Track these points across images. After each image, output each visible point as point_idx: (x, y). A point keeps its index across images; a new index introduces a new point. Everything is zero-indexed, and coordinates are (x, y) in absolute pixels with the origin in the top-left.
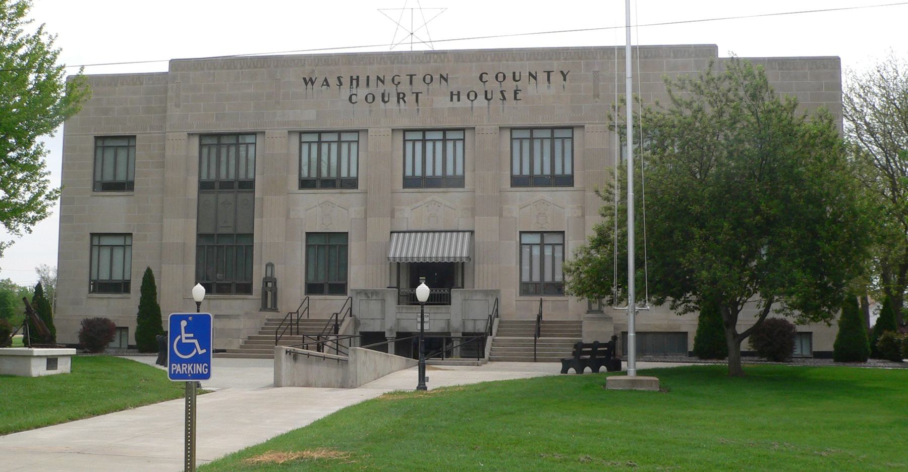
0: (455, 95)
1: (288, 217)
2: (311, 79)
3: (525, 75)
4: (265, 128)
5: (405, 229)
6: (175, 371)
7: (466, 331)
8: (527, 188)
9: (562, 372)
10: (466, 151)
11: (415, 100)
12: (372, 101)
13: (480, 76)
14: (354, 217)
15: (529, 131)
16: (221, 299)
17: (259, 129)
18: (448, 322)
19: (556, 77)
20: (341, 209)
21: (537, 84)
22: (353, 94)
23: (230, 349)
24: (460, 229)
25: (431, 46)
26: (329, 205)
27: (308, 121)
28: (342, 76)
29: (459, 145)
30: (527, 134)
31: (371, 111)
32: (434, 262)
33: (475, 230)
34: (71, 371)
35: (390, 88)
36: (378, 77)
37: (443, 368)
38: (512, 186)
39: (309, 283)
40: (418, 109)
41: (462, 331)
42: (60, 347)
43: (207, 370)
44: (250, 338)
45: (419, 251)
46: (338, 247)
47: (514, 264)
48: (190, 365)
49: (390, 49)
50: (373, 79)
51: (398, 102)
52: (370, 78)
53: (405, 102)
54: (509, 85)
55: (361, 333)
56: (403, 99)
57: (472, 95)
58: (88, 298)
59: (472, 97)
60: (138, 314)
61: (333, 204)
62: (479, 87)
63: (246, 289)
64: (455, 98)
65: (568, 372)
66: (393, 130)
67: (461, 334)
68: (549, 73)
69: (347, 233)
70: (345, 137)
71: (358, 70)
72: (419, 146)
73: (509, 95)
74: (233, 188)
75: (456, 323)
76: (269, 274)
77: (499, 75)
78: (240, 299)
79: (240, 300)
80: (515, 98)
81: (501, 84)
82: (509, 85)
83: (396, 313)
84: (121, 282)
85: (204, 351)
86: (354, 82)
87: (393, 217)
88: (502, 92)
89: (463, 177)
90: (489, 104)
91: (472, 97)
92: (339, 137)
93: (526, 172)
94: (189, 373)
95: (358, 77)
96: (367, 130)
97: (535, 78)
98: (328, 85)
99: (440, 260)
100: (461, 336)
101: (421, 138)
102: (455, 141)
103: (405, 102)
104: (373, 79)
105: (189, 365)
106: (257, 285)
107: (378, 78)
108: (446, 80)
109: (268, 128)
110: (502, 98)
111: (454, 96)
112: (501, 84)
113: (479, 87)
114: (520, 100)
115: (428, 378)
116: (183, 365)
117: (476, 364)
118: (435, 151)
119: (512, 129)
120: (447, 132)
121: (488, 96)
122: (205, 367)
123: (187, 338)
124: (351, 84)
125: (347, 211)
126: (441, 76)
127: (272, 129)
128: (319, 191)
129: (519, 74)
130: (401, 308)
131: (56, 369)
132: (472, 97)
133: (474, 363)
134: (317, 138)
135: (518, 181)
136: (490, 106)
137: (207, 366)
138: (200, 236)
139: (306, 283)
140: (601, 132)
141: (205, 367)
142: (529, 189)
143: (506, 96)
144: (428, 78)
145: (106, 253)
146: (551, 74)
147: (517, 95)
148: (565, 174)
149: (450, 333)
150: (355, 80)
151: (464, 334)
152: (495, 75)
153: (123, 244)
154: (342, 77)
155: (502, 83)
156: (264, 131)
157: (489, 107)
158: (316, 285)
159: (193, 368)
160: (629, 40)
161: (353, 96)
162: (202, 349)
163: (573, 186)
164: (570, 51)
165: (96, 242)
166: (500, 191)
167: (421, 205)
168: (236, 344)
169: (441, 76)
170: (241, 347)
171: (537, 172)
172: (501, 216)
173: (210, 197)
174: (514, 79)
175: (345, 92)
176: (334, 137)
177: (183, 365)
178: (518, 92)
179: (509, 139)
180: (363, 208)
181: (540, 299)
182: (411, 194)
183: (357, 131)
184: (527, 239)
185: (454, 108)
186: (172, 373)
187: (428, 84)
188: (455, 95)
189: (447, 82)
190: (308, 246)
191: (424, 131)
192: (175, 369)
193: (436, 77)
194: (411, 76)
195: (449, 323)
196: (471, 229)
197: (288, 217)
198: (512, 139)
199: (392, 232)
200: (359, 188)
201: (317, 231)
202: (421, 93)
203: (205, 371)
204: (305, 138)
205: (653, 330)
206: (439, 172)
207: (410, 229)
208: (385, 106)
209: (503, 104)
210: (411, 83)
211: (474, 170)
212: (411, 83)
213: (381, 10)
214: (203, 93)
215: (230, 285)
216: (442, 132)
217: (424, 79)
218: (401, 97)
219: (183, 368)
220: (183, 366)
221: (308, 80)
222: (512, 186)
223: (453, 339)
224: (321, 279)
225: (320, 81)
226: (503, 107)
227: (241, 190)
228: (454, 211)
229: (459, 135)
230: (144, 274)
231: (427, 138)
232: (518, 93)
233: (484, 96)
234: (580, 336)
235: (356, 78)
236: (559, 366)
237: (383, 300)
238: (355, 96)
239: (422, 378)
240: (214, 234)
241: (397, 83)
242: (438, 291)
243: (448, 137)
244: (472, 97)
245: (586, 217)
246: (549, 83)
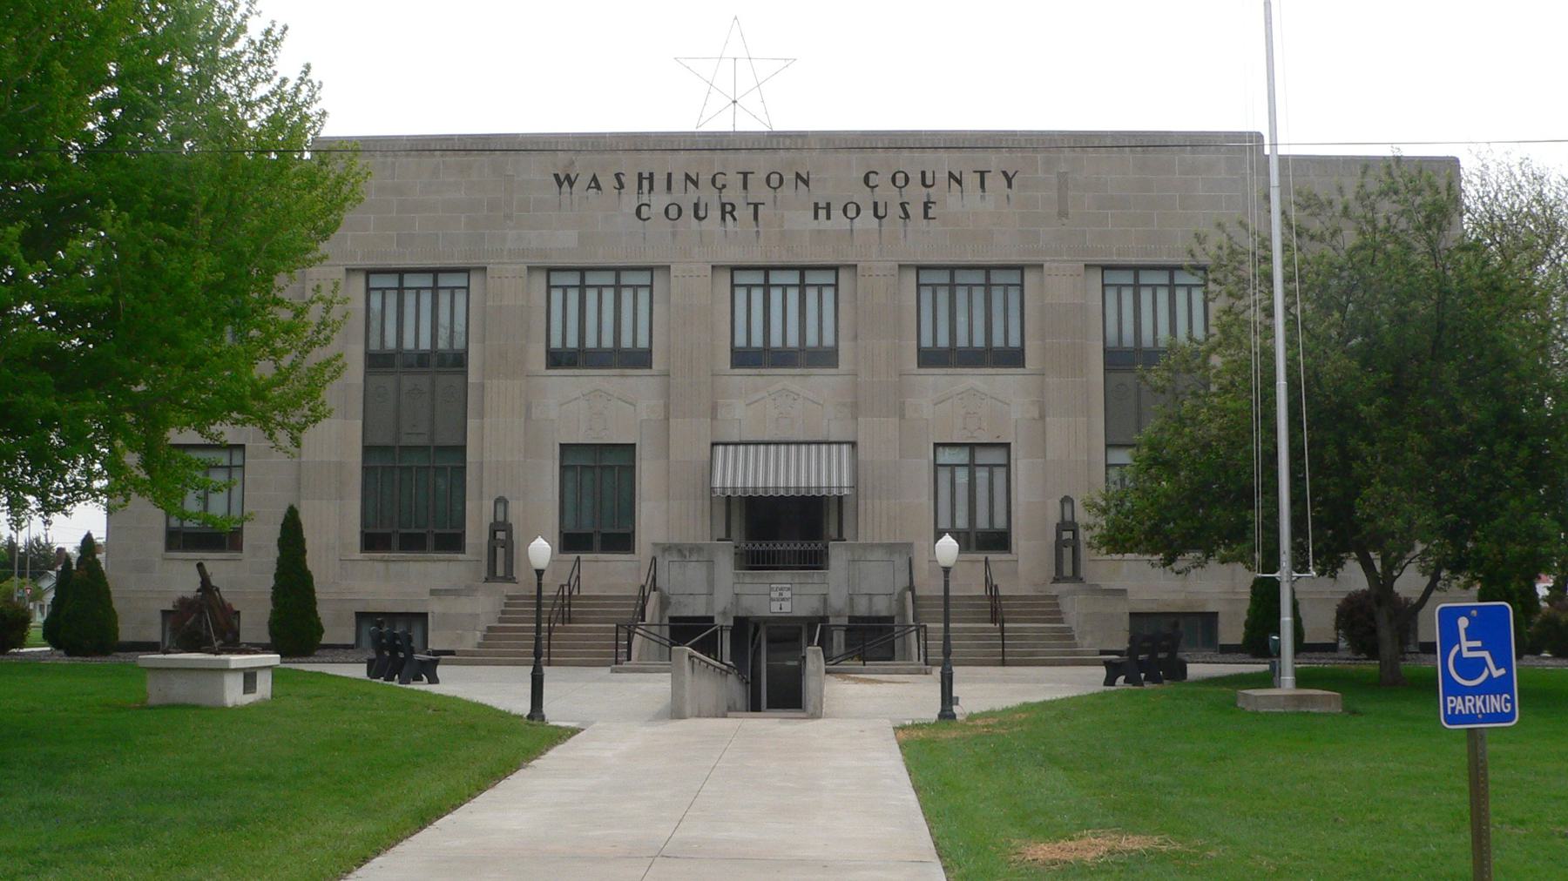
1: (528, 417)
2: (568, 177)
3: (942, 176)
5: (736, 439)
6: (1453, 709)
7: (857, 614)
8: (572, 371)
9: (1105, 684)
10: (840, 305)
11: (752, 217)
12: (676, 217)
13: (865, 177)
14: (646, 418)
15: (948, 272)
16: (409, 561)
17: (473, 262)
18: (825, 598)
19: (995, 182)
20: (628, 405)
21: (962, 192)
23: (461, 649)
24: (832, 439)
25: (768, 124)
26: (601, 396)
27: (564, 248)
28: (623, 172)
29: (828, 294)
30: (944, 277)
31: (674, 234)
32: (771, 496)
33: (859, 441)
34: (272, 696)
35: (708, 195)
36: (950, 173)
37: (884, 679)
38: (919, 366)
39: (566, 532)
40: (758, 232)
41: (848, 614)
42: (248, 652)
43: (1509, 705)
44: (490, 629)
45: (808, 478)
46: (617, 468)
47: (926, 501)
48: (1479, 697)
49: (697, 128)
50: (678, 178)
51: (723, 218)
52: (674, 177)
53: (735, 219)
54: (916, 193)
55: (672, 619)
56: (731, 213)
57: (851, 209)
58: (166, 559)
59: (852, 212)
60: (273, 588)
61: (609, 395)
62: (863, 196)
63: (452, 542)
64: (822, 213)
65: (1117, 684)
66: (713, 267)
67: (847, 619)
68: (982, 174)
69: (634, 445)
70: (627, 278)
71: (648, 163)
72: (757, 295)
73: (916, 210)
74: (393, 366)
75: (838, 601)
76: (500, 518)
77: (897, 175)
78: (444, 561)
79: (442, 563)
80: (926, 216)
81: (901, 192)
82: (916, 193)
83: (734, 583)
85: (1502, 671)
86: (646, 183)
87: (714, 417)
88: (903, 205)
89: (650, 351)
90: (880, 226)
91: (852, 213)
92: (583, 279)
93: (943, 341)
94: (1478, 712)
95: (651, 175)
96: (669, 267)
97: (959, 182)
98: (598, 187)
99: (803, 492)
100: (847, 623)
101: (762, 281)
102: (820, 287)
103: (735, 219)
104: (678, 178)
105: (1477, 697)
106: (476, 533)
107: (688, 177)
108: (806, 182)
109: (492, 261)
110: (903, 216)
111: (820, 211)
112: (901, 192)
113: (863, 196)
114: (934, 218)
115: (957, 698)
116: (1467, 698)
117: (923, 671)
118: (784, 304)
119: (920, 268)
120: (406, 276)
121: (879, 210)
122: (1506, 700)
123: (1470, 649)
124: (640, 186)
125: (632, 408)
126: (798, 176)
127: (499, 263)
128: (583, 372)
129: (932, 175)
130: (742, 575)
131: (254, 692)
132: (852, 213)
133: (921, 669)
134: (763, 278)
135: (930, 358)
136: (883, 228)
137: (1508, 697)
138: (368, 450)
139: (561, 532)
140: (1071, 275)
141: (1507, 701)
142: (950, 371)
144: (775, 179)
146: (986, 175)
147: (930, 211)
148: (638, 346)
149: (828, 617)
150: (646, 180)
151: (852, 619)
152: (891, 176)
153: (228, 464)
154: (623, 174)
155: (903, 189)
156: (1040, 263)
157: (880, 231)
158: (579, 535)
159: (1484, 702)
160: (1273, 123)
161: (643, 208)
162: (1498, 668)
163: (1023, 366)
164: (1018, 137)
166: (900, 375)
167: (763, 398)
168: (472, 640)
169: (798, 176)
170: (480, 645)
171: (962, 342)
172: (902, 416)
173: (387, 382)
174: (924, 184)
175: (630, 200)
176: (609, 278)
177: (1467, 698)
178: (930, 205)
179: (915, 285)
180: (662, 402)
181: (984, 559)
182: (746, 378)
183: (651, 269)
184: (946, 456)
185: (819, 231)
186: (1449, 713)
187: (775, 188)
188: (821, 208)
189: (808, 186)
190: (563, 468)
191: (767, 269)
192: (1453, 705)
193: (789, 177)
194: (745, 175)
195: (825, 601)
196: (851, 439)
197: (528, 417)
198: (919, 286)
199: (714, 444)
200: (654, 366)
201: (580, 442)
202: (763, 204)
203: (1506, 707)
204: (557, 279)
205: (1161, 610)
206: (793, 341)
207: (745, 438)
208: (700, 225)
209: (905, 225)
210: (745, 187)
211: (856, 337)
212: (745, 187)
213: (681, 60)
214: (373, 198)
215: (423, 536)
216: (432, 275)
217: (894, 180)
218: (727, 210)
219: (1467, 704)
220: (1467, 701)
221: (562, 178)
222: (733, 366)
223: (833, 628)
224: (587, 527)
225: (583, 181)
226: (905, 231)
228: (820, 407)
229: (643, 278)
230: (283, 517)
231: (587, 283)
232: (930, 208)
233: (872, 212)
234: (1061, 621)
235: (648, 176)
236: (1102, 672)
237: (711, 562)
238: (647, 207)
239: (948, 698)
240: (394, 447)
241: (720, 186)
242: (813, 545)
243: (808, 281)
244: (852, 212)
245: (1048, 419)
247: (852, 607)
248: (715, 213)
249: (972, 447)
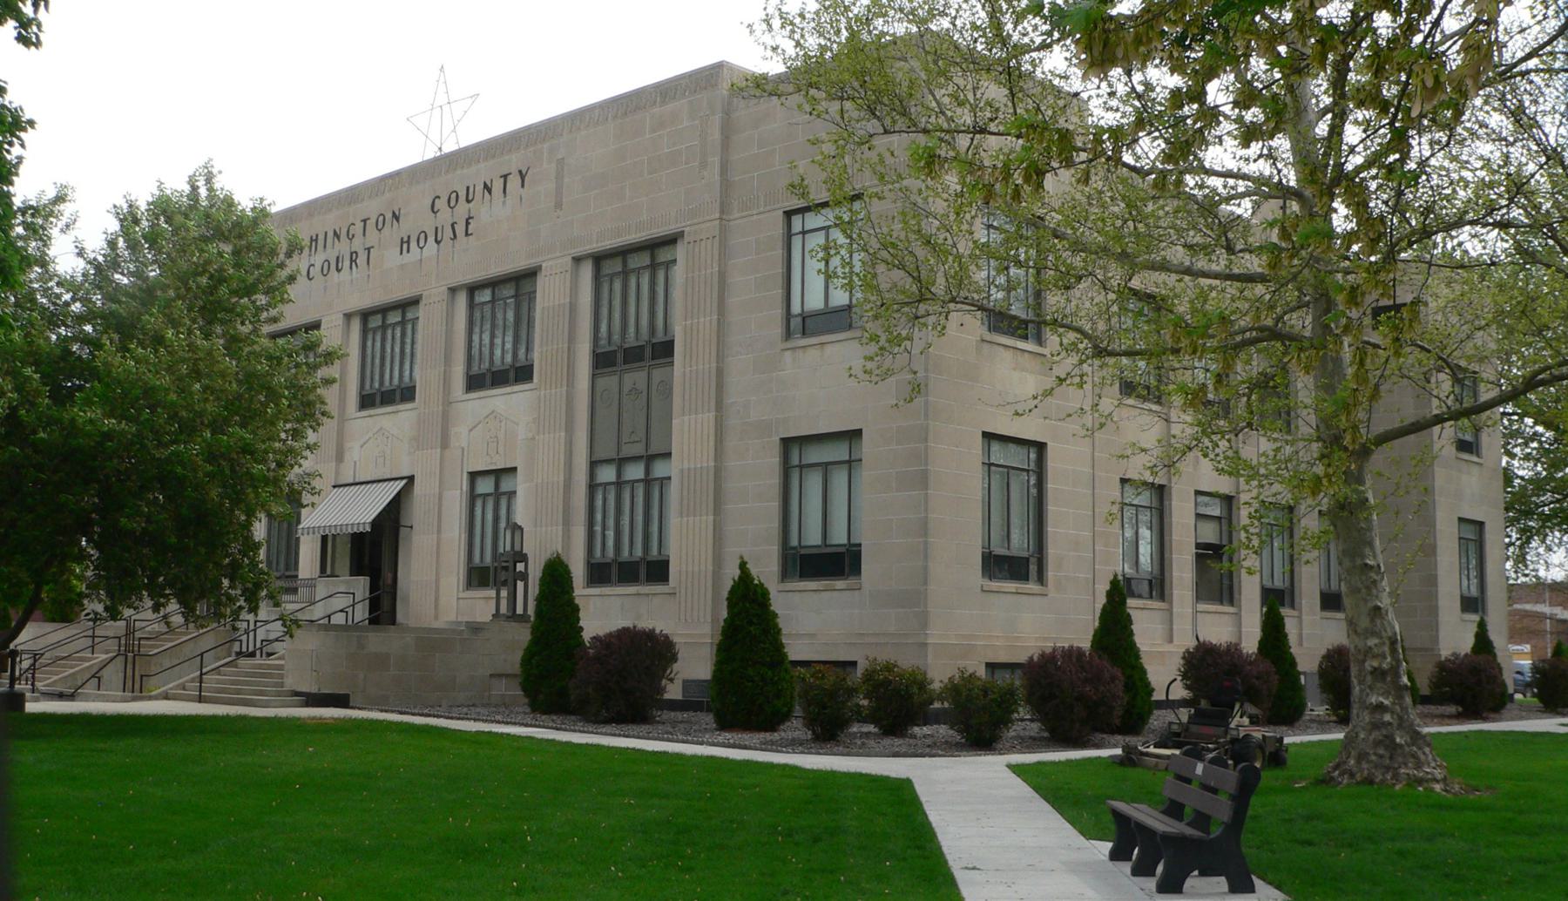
4: (684, 224)
84: (842, 550)
90: (453, 246)
128: (517, 388)
145: (814, 482)
173: (609, 382)
210: (364, 235)
227: (627, 366)
246: (505, 196)
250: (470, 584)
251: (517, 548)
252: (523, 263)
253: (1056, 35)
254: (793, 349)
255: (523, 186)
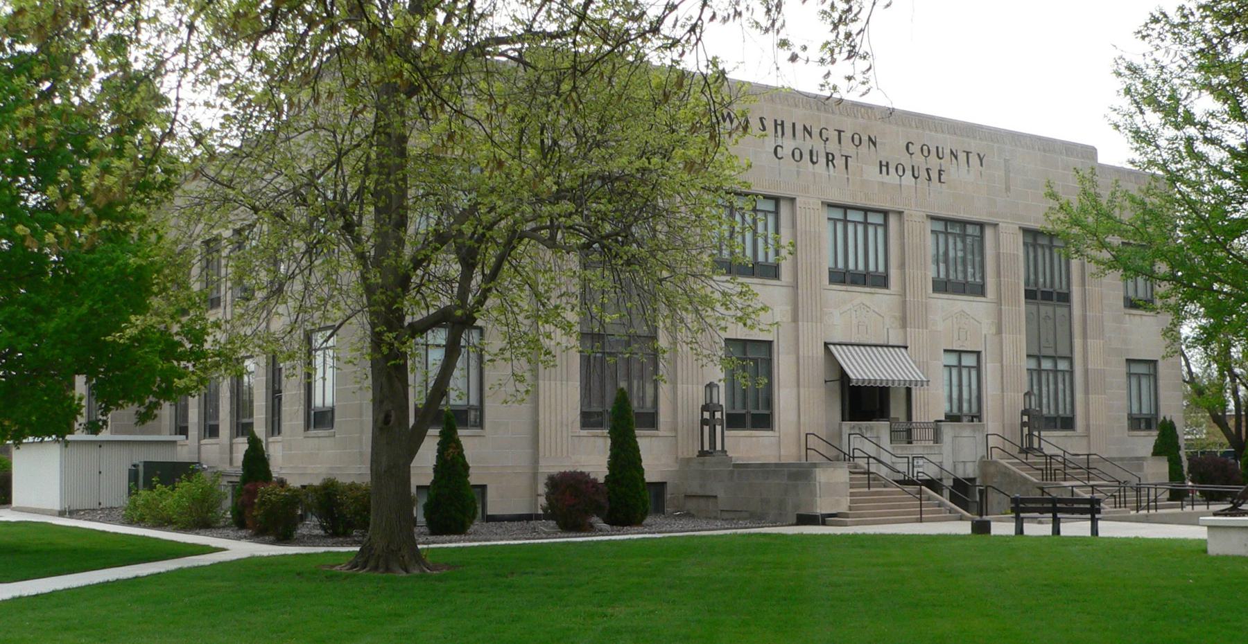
0: (884, 166)
15: (863, 213)
19: (974, 160)
22: (778, 146)
31: (798, 173)
40: (848, 178)
51: (828, 165)
52: (797, 127)
56: (832, 161)
62: (946, 162)
78: (648, 436)
88: (927, 170)
90: (916, 184)
95: (783, 122)
143: (931, 176)
165: (969, 360)
175: (770, 143)
210: (840, 142)
218: (830, 158)
221: (725, 115)
224: (739, 410)
246: (969, 166)
247: (955, 470)
248: (823, 160)
249: (960, 352)
250: (585, 425)
251: (1027, 407)
252: (985, 218)
253: (473, 27)
254: (1130, 314)
255: (982, 165)
